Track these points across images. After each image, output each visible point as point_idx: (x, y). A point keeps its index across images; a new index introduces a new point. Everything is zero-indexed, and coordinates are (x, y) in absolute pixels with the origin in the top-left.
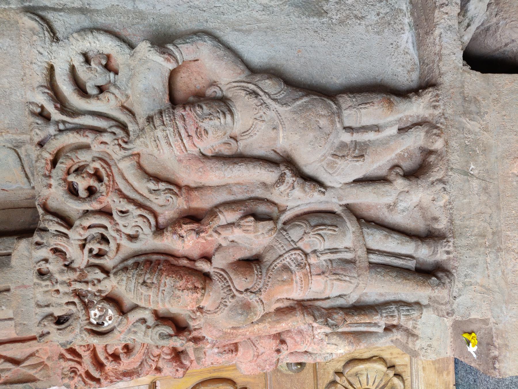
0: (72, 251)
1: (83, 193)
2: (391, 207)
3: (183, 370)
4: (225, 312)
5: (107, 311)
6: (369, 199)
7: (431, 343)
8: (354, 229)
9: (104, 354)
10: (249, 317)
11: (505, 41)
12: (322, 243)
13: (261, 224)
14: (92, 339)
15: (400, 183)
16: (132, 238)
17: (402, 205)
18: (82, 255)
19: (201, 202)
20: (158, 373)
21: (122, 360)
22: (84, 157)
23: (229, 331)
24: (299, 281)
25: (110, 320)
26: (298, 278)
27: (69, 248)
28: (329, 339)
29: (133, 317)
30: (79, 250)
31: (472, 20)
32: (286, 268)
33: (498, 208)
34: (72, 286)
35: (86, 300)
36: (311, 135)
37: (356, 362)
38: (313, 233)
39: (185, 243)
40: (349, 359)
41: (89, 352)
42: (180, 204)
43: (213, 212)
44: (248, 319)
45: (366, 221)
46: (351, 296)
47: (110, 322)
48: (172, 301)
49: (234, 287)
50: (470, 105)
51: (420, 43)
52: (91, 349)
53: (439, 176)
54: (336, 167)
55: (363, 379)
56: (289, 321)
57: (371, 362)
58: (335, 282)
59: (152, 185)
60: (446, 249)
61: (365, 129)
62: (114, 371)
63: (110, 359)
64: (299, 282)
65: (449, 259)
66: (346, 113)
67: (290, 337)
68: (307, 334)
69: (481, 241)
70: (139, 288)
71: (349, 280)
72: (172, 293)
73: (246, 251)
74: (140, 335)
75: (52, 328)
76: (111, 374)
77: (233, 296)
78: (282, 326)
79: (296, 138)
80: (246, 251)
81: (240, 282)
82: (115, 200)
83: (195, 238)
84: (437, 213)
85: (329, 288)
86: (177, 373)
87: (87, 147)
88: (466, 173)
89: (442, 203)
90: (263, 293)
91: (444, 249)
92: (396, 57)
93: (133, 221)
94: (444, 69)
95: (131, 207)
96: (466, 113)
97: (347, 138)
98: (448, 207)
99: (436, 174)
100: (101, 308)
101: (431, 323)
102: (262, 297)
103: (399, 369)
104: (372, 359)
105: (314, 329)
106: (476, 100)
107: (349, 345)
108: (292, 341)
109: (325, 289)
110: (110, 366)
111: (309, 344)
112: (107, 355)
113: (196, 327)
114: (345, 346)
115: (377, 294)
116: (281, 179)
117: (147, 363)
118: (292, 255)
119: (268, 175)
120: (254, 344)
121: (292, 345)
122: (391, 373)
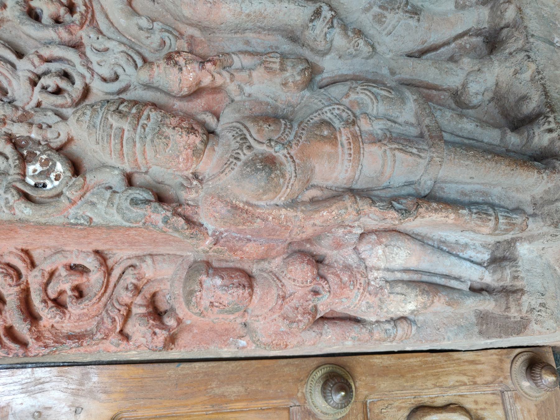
3: (164, 332)
4: (237, 169)
5: (54, 165)
7: (544, 301)
8: (415, 97)
9: (42, 295)
10: (273, 176)
12: (375, 104)
14: (23, 205)
18: (30, 92)
20: (123, 340)
21: (69, 309)
23: (241, 205)
24: (345, 143)
25: (56, 179)
26: (344, 138)
27: (14, 82)
28: (391, 287)
30: (28, 85)
34: (7, 126)
35: (25, 153)
37: (426, 410)
38: (361, 87)
40: (414, 406)
41: (17, 289)
44: (273, 179)
46: (423, 182)
47: (56, 183)
48: (156, 141)
49: (251, 136)
52: (22, 286)
53: (520, 44)
54: (385, 22)
56: (334, 207)
57: (448, 411)
58: (397, 152)
60: (546, 126)
62: (54, 332)
63: (50, 304)
64: (346, 146)
65: (552, 141)
67: (332, 273)
68: (359, 272)
70: (109, 117)
71: (417, 153)
72: (158, 129)
73: (269, 107)
76: (47, 334)
77: (250, 147)
78: (323, 216)
80: (269, 107)
82: (91, 36)
83: (197, 70)
84: (523, 90)
85: (390, 163)
86: (155, 337)
89: (527, 76)
90: (294, 146)
91: (542, 129)
98: (538, 78)
100: (46, 159)
101: (539, 271)
102: (293, 152)
104: (449, 407)
105: (368, 269)
107: (423, 294)
108: (337, 280)
109: (383, 166)
110: (48, 316)
111: (361, 291)
112: (46, 298)
113: (190, 202)
114: (417, 296)
115: (457, 192)
117: (108, 314)
118: (334, 109)
120: (278, 278)
121: (336, 287)
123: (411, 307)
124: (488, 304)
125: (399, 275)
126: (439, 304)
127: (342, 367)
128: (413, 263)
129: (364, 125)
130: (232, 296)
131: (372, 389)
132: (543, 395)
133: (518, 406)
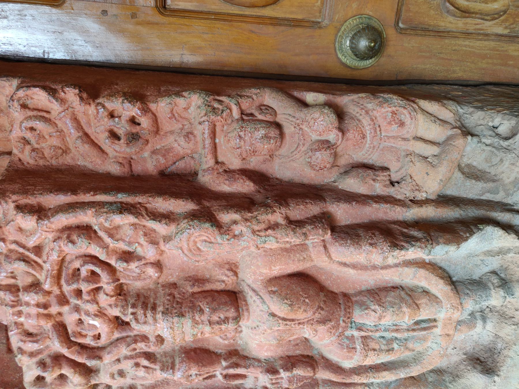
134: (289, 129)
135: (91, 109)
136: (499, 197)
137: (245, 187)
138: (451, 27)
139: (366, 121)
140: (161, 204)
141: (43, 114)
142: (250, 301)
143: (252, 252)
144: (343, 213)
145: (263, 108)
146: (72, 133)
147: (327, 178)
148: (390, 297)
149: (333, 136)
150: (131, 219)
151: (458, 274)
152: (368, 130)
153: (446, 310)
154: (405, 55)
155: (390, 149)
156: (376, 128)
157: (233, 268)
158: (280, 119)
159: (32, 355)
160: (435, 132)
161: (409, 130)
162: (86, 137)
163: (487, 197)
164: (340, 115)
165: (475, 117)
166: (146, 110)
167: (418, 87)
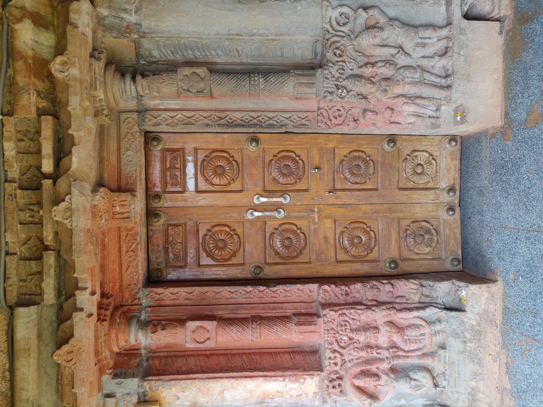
0: (334, 72)
1: (338, 55)
2: (433, 67)
6: (425, 63)
11: (479, 10)
13: (391, 66)
15: (437, 58)
16: (351, 70)
17: (437, 66)
19: (372, 60)
22: (338, 45)
29: (351, 93)
31: (467, 2)
32: (398, 80)
33: (470, 66)
36: (409, 38)
39: (367, 71)
42: (366, 60)
43: (376, 63)
45: (424, 70)
50: (462, 31)
51: (448, 10)
55: (419, 158)
59: (358, 54)
61: (426, 38)
66: (420, 33)
69: (463, 77)
74: (353, 99)
75: (328, 94)
79: (404, 39)
81: (384, 83)
87: (339, 42)
88: (459, 54)
89: (450, 64)
92: (439, 15)
93: (353, 65)
94: (454, 19)
95: (351, 60)
96: (460, 34)
97: (419, 41)
99: (449, 54)
103: (435, 157)
106: (465, 29)
110: (333, 120)
116: (399, 52)
119: (394, 51)
122: (431, 158)
123: (412, 120)
124: (433, 120)
125: (411, 113)
126: (420, 120)
127: (394, 138)
128: (415, 110)
129: (406, 80)
130: (374, 116)
131: (401, 145)
132: (451, 149)
133: (444, 152)
134: (381, 289)
135: (337, 289)
136: (434, 301)
137: (374, 303)
138: (416, 258)
139: (398, 286)
140: (359, 307)
141: (326, 291)
142: (380, 328)
143: (379, 316)
144: (397, 306)
145: (374, 285)
146: (333, 295)
147: (392, 300)
148: (413, 327)
149: (391, 290)
150: (354, 310)
151: (428, 321)
152: (399, 288)
153: (426, 330)
154: (405, 267)
155: (405, 292)
156: (401, 287)
157: (375, 321)
158: (379, 287)
159: (330, 349)
160: (415, 287)
161: (409, 287)
162: (336, 295)
163: (431, 301)
164: (392, 285)
165: (424, 282)
166: (349, 288)
167: (410, 275)
